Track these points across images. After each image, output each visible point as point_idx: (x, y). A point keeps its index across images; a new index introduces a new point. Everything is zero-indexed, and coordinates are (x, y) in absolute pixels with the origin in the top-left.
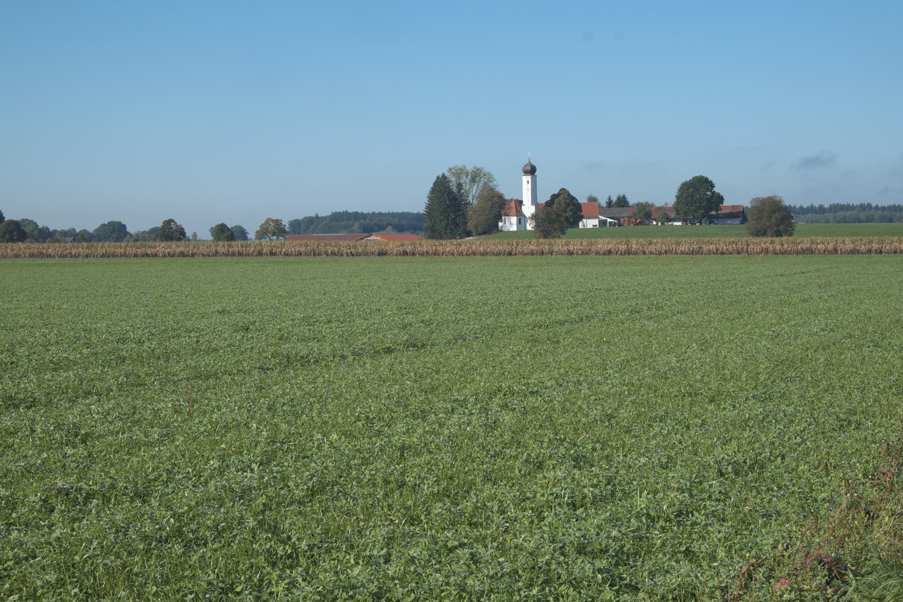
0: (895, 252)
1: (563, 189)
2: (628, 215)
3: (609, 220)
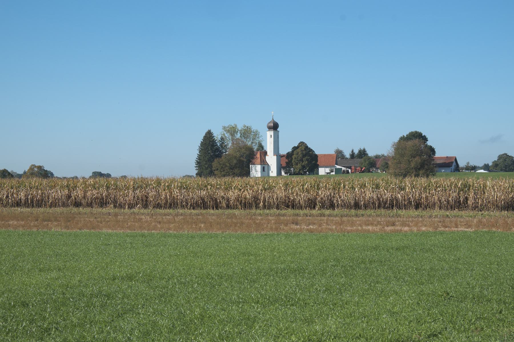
0: (357, 206)
1: (301, 142)
3: (343, 168)
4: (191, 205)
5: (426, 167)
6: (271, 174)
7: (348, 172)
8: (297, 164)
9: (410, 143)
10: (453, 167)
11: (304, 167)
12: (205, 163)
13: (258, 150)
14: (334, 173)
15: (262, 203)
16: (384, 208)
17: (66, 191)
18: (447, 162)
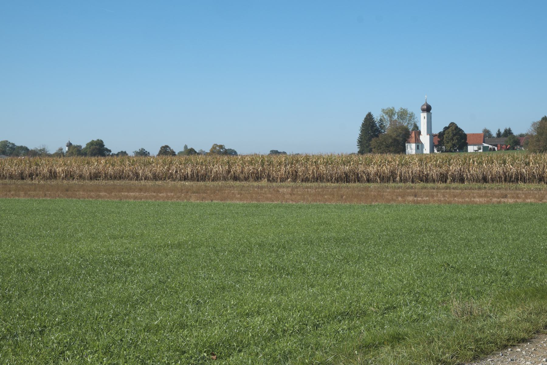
3: (490, 146)
4: (335, 179)
6: (425, 152)
7: (494, 150)
11: (454, 145)
13: (413, 130)
14: (481, 151)
15: (398, 177)
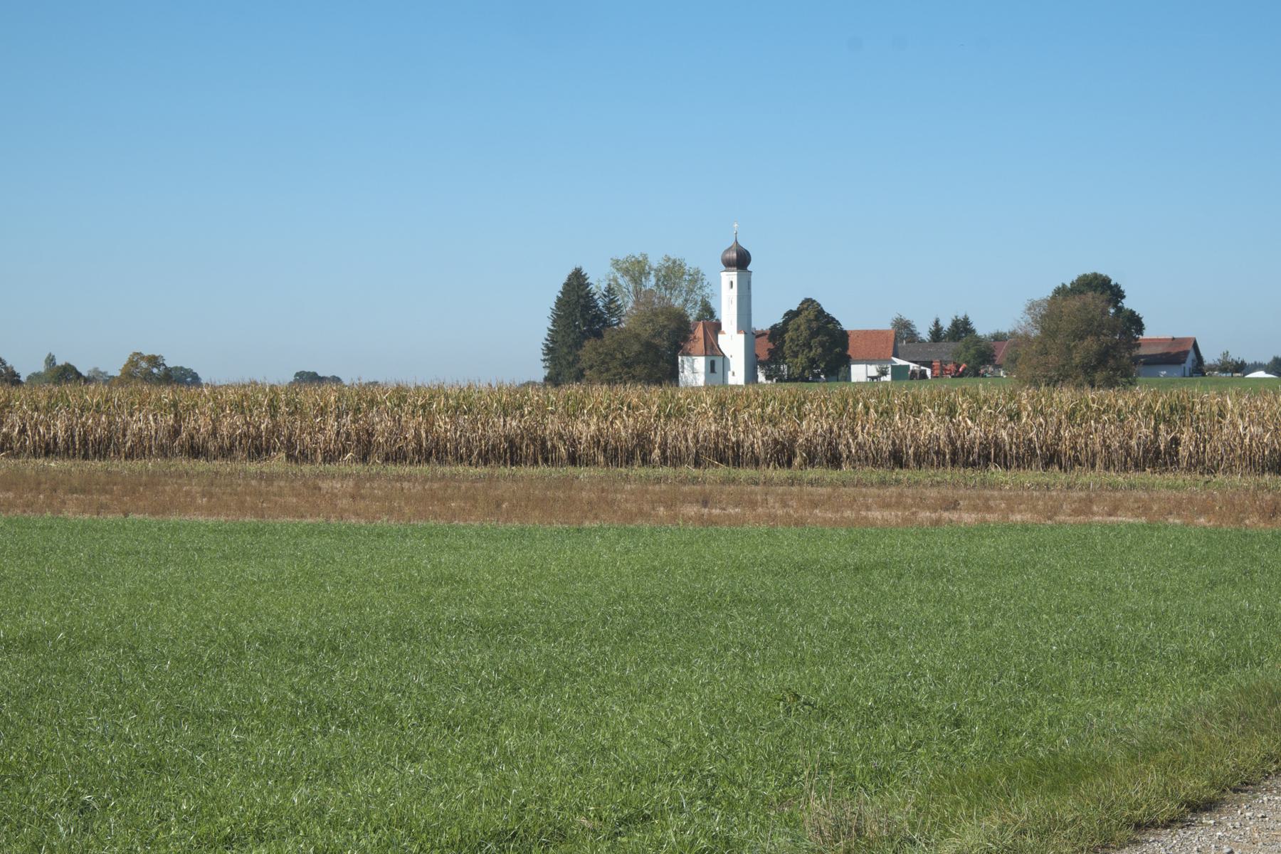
0: (897, 459)
2: (964, 351)
3: (913, 366)
4: (480, 454)
5: (1111, 362)
6: (732, 380)
7: (923, 375)
8: (795, 355)
9: (1075, 303)
10: (1189, 363)
11: (812, 362)
12: (565, 350)
13: (698, 319)
14: (888, 378)
15: (657, 451)
16: (966, 464)
17: (170, 419)
18: (1174, 351)
